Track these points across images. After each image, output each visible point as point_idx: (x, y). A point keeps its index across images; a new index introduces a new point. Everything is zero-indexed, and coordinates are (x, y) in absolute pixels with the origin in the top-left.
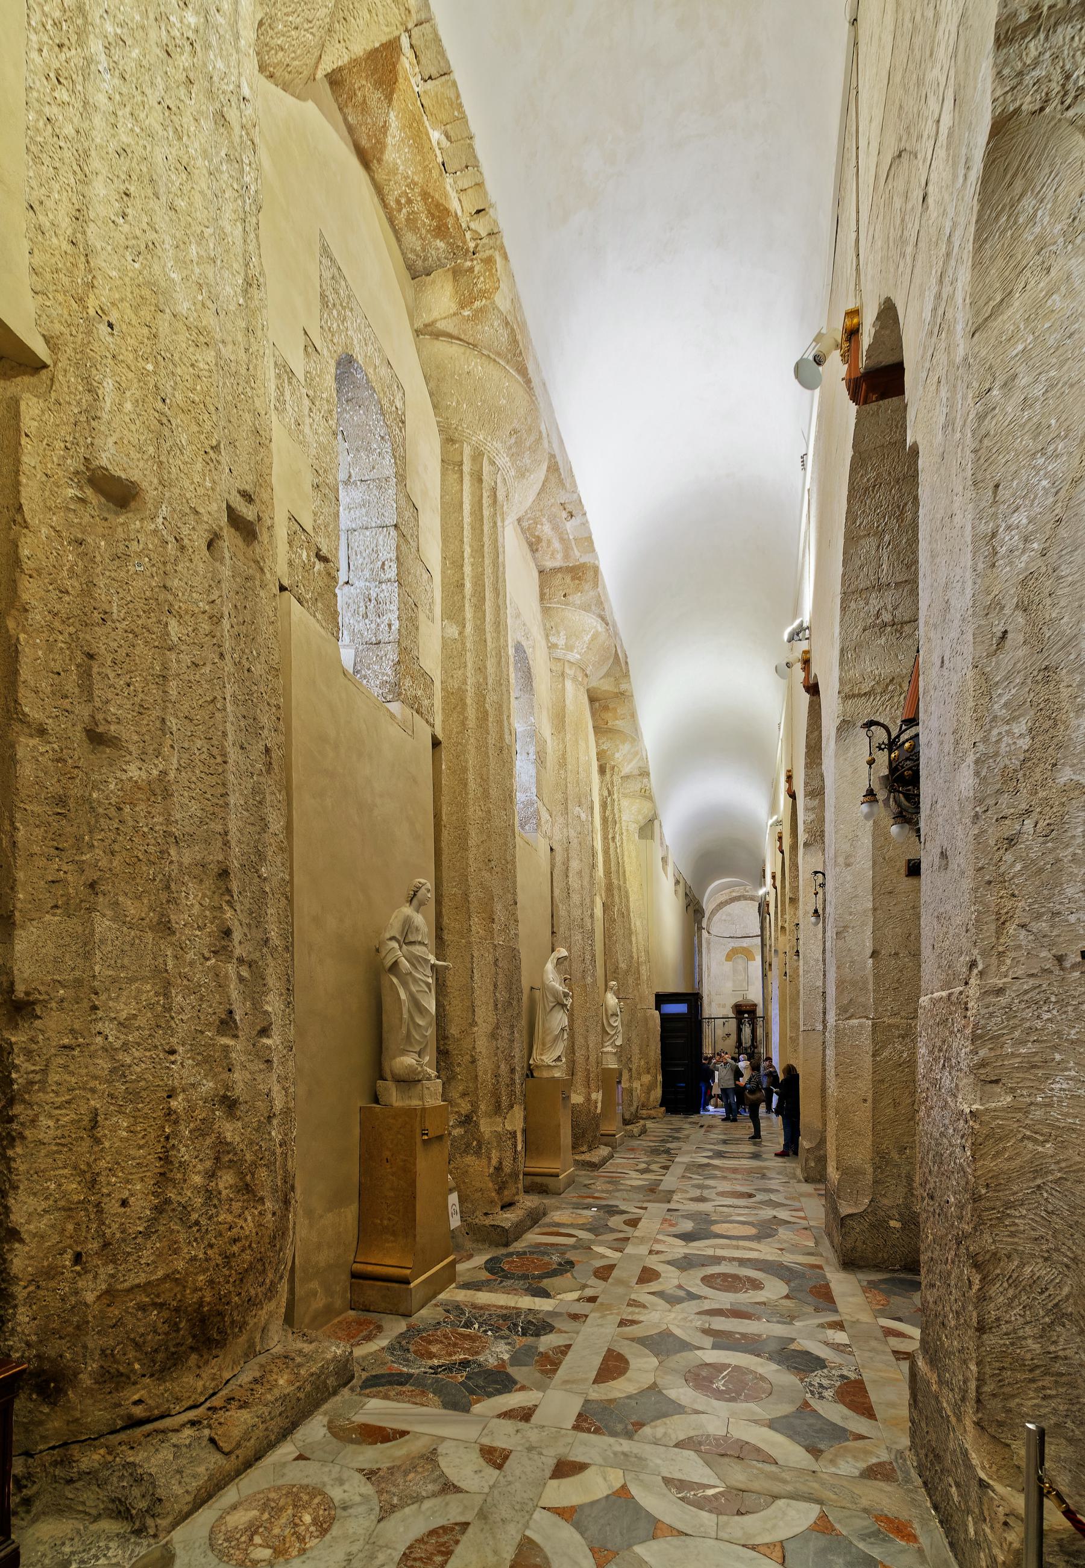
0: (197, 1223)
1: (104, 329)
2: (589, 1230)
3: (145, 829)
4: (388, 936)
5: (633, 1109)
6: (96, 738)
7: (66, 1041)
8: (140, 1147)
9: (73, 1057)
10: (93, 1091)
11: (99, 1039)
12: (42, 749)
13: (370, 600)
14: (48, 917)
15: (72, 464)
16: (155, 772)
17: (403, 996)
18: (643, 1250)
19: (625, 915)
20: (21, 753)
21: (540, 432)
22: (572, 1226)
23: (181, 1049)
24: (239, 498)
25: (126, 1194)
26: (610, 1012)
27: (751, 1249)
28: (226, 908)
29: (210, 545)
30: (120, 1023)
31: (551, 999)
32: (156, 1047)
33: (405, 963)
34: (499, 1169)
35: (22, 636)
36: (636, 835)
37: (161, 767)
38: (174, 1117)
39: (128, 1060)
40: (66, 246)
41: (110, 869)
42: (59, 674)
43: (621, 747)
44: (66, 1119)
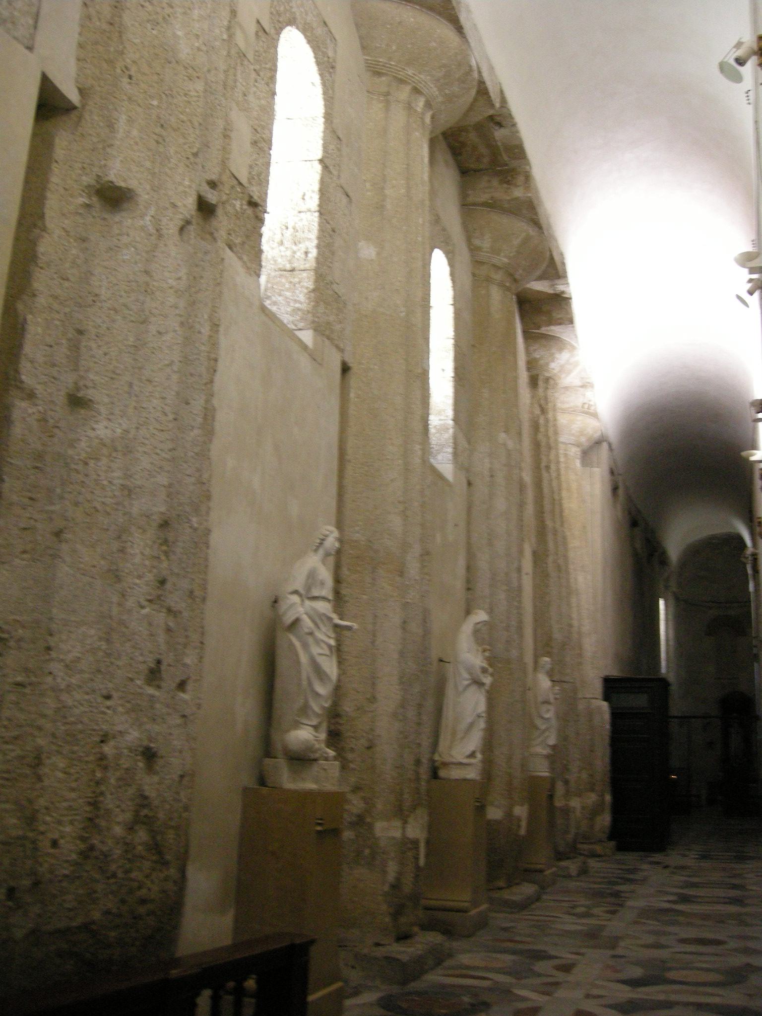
0: (114, 875)
1: (125, 80)
2: (509, 974)
3: (105, 483)
4: (291, 589)
5: (570, 837)
6: (76, 402)
7: (19, 679)
8: (73, 790)
9: (24, 695)
10: (40, 728)
11: (49, 679)
12: (30, 411)
13: (287, 228)
14: (17, 561)
15: (87, 180)
16: (119, 431)
17: (304, 659)
18: (579, 994)
19: (562, 569)
20: (16, 414)
21: (470, 66)
22: (486, 969)
23: (115, 695)
24: (207, 188)
25: (56, 836)
26: (540, 699)
27: (712, 995)
28: (163, 558)
29: (182, 229)
30: (67, 666)
31: (466, 675)
32: (94, 691)
33: (307, 623)
34: (396, 886)
35: (29, 317)
36: (578, 463)
37: (125, 426)
38: (105, 762)
39: (70, 702)
40: (105, 26)
41: (73, 519)
42: (51, 346)
43: (557, 356)
44: (13, 754)
